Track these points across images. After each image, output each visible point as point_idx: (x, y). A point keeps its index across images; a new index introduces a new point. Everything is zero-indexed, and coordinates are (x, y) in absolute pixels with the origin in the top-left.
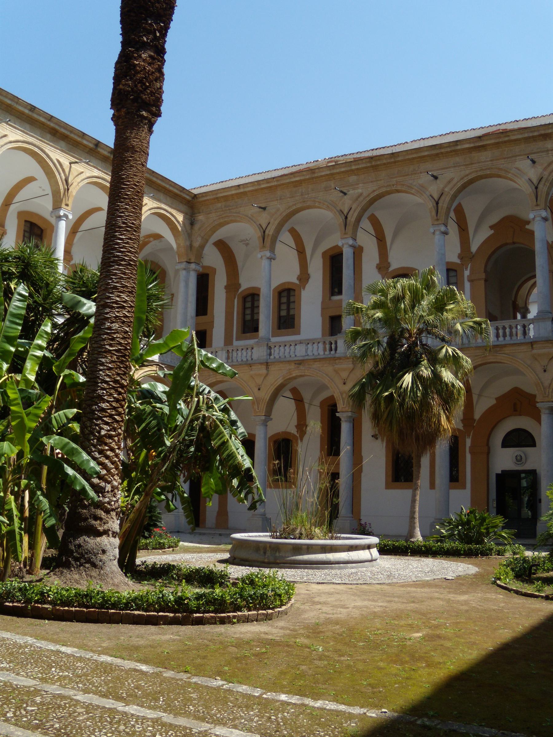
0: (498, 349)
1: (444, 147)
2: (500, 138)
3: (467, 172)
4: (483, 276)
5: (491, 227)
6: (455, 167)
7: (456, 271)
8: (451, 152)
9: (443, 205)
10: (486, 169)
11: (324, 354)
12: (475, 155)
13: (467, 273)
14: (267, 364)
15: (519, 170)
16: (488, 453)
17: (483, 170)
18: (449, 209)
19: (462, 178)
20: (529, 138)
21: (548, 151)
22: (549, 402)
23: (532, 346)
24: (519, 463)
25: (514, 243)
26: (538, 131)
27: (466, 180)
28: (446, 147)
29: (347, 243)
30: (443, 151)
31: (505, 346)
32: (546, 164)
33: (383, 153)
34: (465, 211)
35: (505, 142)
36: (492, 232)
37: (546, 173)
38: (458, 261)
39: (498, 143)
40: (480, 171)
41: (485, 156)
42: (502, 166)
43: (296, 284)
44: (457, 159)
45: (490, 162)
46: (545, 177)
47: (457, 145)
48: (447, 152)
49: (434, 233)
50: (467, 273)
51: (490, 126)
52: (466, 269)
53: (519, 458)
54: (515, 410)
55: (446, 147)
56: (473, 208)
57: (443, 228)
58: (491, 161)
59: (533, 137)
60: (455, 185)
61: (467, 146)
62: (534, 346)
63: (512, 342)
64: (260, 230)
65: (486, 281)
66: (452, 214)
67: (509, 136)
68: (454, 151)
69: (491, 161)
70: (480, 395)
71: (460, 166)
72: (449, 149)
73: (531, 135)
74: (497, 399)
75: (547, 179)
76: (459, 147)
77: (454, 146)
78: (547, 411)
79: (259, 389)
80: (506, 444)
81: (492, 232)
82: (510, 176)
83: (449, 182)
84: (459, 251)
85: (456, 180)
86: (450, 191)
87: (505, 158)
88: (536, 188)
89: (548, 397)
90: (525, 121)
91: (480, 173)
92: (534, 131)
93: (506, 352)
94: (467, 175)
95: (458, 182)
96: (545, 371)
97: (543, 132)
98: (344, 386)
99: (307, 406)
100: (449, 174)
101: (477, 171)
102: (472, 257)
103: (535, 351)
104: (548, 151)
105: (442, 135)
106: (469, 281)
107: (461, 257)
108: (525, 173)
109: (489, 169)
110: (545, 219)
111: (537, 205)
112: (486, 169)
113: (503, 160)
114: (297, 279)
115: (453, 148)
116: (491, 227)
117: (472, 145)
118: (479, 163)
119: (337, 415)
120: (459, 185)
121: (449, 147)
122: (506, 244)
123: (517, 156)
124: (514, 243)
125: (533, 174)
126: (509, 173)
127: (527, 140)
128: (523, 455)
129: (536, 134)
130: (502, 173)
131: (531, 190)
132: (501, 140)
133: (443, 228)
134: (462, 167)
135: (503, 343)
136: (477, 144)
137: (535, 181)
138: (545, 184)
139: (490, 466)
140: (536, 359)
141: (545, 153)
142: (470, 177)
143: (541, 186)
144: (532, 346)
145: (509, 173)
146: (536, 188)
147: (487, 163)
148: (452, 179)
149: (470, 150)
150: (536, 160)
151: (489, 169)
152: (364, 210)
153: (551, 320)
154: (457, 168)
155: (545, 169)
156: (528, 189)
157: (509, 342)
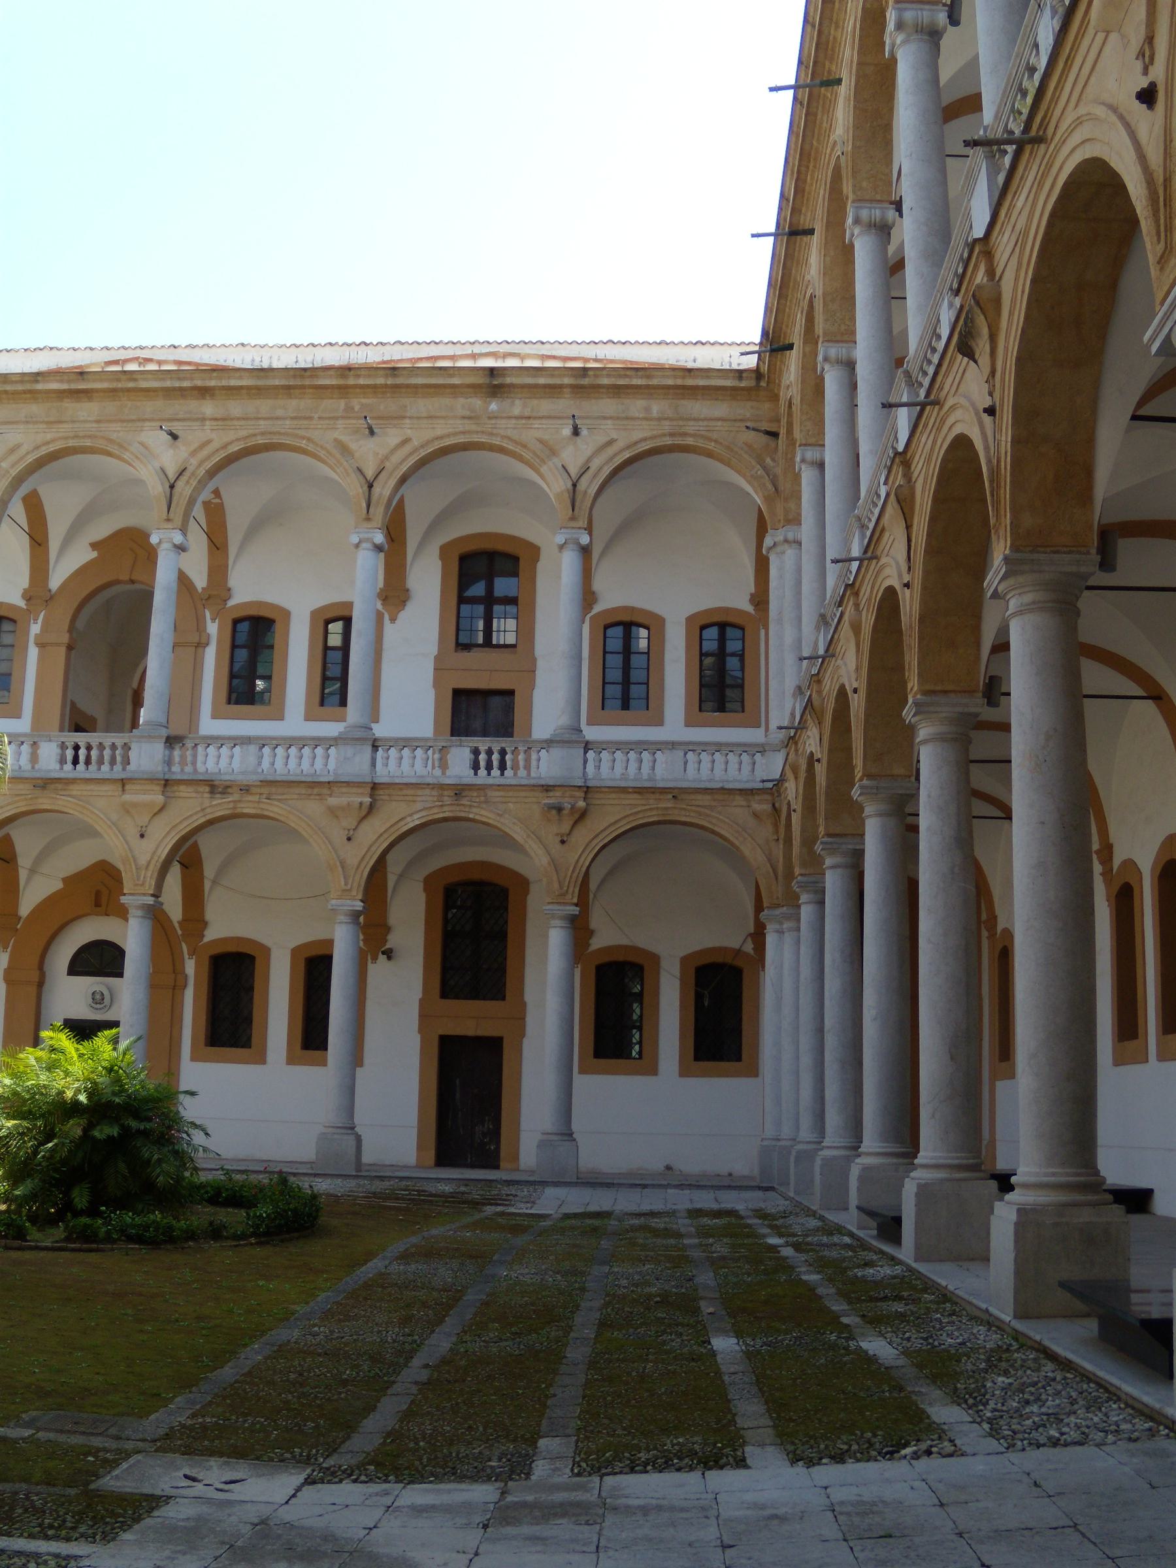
0: (60, 786)
1: (13, 382)
2: (118, 380)
3: (49, 437)
4: (65, 639)
5: (94, 546)
6: (27, 422)
7: (14, 621)
8: (25, 392)
9: (184, 489)
10: (84, 437)
11: (182, 770)
12: (69, 405)
13: (35, 629)
14: (167, 783)
15: (146, 448)
16: (41, 984)
17: (76, 437)
18: (191, 502)
19: (37, 448)
20: (174, 389)
21: (204, 419)
22: (144, 895)
23: (123, 786)
24: (98, 1006)
25: (132, 582)
26: (192, 379)
27: (44, 451)
28: (16, 382)
29: (170, 541)
30: (8, 388)
31: (73, 781)
32: (196, 445)
33: (230, 363)
34: (46, 508)
35: (129, 390)
36: (95, 554)
37: (194, 462)
38: (22, 604)
39: (114, 390)
40: (73, 438)
41: (87, 411)
42: (114, 436)
43: (20, 608)
44: (35, 409)
45: (95, 425)
46: (191, 469)
47: (37, 381)
48: (15, 393)
49: (357, 546)
50: (35, 629)
51: (399, 342)
52: (36, 620)
53: (98, 997)
54: (98, 904)
55: (16, 382)
56: (62, 504)
57: (178, 538)
58: (98, 422)
59: (181, 389)
60: (22, 458)
61: (54, 386)
62: (127, 787)
63: (88, 776)
64: (162, 484)
65: (70, 648)
66: (198, 511)
67: (135, 380)
68: (30, 392)
69: (98, 422)
70: (32, 871)
71: (37, 422)
72: (20, 387)
73: (177, 384)
74: (64, 880)
75: (193, 474)
76: (40, 386)
77: (29, 381)
78: (140, 913)
79: (142, 836)
80: (78, 966)
81: (95, 554)
82: (126, 456)
83: (12, 451)
84: (26, 585)
85: (22, 451)
86: (199, 466)
87: (123, 421)
88: (172, 487)
89: (143, 885)
90: (522, 345)
91: (71, 443)
92: (184, 379)
93: (74, 793)
94: (48, 443)
95: (28, 453)
96: (142, 836)
97: (199, 383)
98: (145, 840)
99: (23, 875)
100: (193, 435)
101: (67, 438)
102: (50, 599)
103: (127, 797)
104: (204, 419)
105: (459, 342)
106: (37, 644)
107: (28, 596)
108: (155, 455)
109: (90, 437)
110: (379, 548)
111: (168, 520)
112: (84, 437)
113: (119, 424)
114: (23, 596)
115: (28, 387)
116: (94, 546)
117: (65, 386)
118: (73, 422)
119: (123, 899)
120: (30, 459)
121: (22, 382)
122: (117, 582)
123: (144, 420)
124: (132, 582)
125: (169, 458)
126: (126, 450)
127: (168, 393)
128: (106, 993)
129: (186, 384)
130: (114, 449)
131: (160, 489)
132: (120, 386)
133: (178, 538)
134: (41, 426)
135: (71, 776)
136: (74, 386)
137: (172, 476)
138: (188, 482)
139: (43, 1011)
140: (128, 812)
141: (198, 423)
142: (52, 448)
143: (180, 485)
144: (123, 786)
145: (126, 450)
146: (172, 487)
147: (87, 425)
148: (18, 446)
149: (62, 394)
150: (179, 433)
151: (90, 437)
152: (19, 480)
153: (164, 740)
154: (31, 426)
155: (193, 453)
156: (157, 488)
157: (82, 776)
